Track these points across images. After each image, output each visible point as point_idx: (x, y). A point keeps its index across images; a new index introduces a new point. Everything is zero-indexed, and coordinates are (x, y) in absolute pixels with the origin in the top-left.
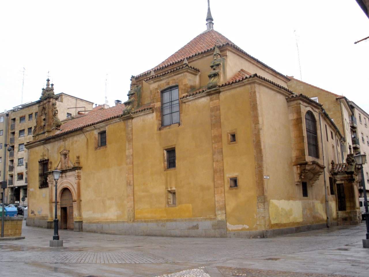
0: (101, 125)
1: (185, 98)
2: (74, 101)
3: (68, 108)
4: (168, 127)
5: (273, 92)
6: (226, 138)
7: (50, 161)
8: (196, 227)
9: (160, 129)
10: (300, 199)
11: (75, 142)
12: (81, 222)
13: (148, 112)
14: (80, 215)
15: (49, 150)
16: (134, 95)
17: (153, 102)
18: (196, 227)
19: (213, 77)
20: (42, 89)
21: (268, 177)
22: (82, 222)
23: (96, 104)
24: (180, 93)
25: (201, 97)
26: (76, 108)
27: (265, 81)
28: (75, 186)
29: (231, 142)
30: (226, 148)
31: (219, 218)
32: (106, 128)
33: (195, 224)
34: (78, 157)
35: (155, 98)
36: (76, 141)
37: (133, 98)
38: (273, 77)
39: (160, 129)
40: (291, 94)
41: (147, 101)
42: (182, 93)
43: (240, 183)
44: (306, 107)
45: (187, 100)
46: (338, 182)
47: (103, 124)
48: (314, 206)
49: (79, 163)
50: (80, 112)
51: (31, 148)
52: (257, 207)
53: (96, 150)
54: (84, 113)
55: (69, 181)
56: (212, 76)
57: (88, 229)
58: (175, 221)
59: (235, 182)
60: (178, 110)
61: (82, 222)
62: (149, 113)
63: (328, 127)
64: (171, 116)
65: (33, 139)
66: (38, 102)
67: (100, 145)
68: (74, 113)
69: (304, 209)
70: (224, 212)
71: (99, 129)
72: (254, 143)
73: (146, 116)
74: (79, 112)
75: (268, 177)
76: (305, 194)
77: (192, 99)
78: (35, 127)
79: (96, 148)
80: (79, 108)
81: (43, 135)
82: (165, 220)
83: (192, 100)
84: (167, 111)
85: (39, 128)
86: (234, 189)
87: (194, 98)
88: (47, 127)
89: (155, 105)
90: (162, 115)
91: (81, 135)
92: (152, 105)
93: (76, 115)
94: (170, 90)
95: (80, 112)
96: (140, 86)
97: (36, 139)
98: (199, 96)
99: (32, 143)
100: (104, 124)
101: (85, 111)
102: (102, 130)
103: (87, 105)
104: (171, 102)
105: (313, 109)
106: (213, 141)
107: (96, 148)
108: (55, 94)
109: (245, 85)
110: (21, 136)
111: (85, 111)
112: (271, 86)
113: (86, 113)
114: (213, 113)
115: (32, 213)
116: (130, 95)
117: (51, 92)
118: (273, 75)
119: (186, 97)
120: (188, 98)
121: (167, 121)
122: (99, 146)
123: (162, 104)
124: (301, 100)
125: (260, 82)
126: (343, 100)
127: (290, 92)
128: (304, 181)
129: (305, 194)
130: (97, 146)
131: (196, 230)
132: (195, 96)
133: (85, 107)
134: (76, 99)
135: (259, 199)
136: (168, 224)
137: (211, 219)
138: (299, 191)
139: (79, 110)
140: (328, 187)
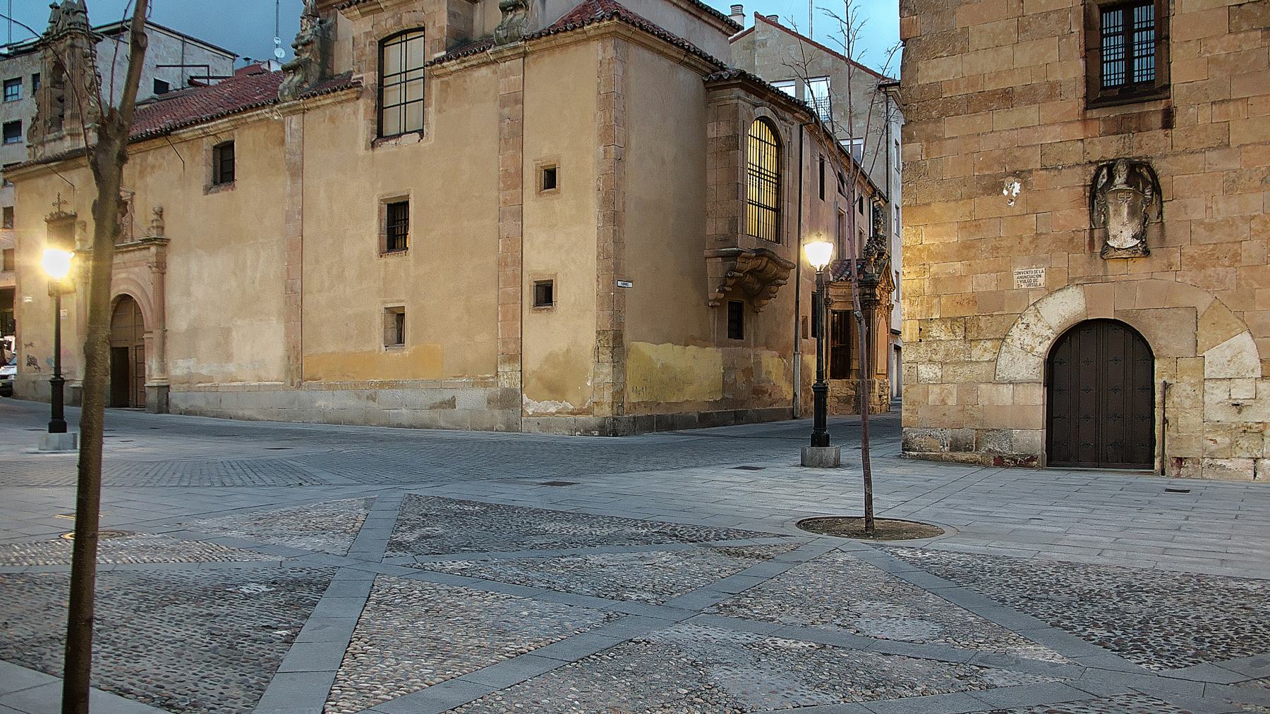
0: (220, 127)
1: (439, 66)
2: (176, 45)
3: (158, 66)
4: (393, 142)
5: (665, 64)
6: (532, 179)
7: (79, 219)
8: (451, 403)
9: (373, 145)
10: (719, 345)
11: (149, 170)
12: (164, 389)
13: (343, 98)
14: (163, 369)
15: (76, 188)
16: (309, 47)
17: (359, 71)
18: (451, 403)
19: (511, 11)
20: (51, 6)
21: (620, 283)
22: (168, 386)
23: (247, 59)
24: (428, 49)
25: (479, 66)
26: (182, 66)
27: (644, 33)
28: (150, 291)
29: (545, 189)
30: (533, 203)
31: (505, 383)
32: (233, 135)
33: (447, 395)
34: (160, 213)
35: (364, 58)
36: (153, 167)
37: (308, 54)
38: (691, 17)
39: (373, 145)
40: (718, 68)
41: (343, 64)
42: (433, 52)
43: (559, 294)
44: (756, 106)
45: (443, 71)
46: (836, 307)
47: (227, 122)
48: (758, 364)
49: (161, 228)
50: (195, 80)
51: (21, 180)
52: (596, 360)
53: (207, 194)
54: (205, 81)
55: (132, 276)
56: (508, 9)
57: (183, 406)
58: (402, 386)
59: (545, 294)
60: (422, 98)
61: (168, 386)
62: (347, 101)
63: (827, 166)
64: (813, 80)
65: (29, 155)
66: (44, 43)
67: (219, 181)
68: (173, 79)
69: (728, 369)
70: (518, 367)
71: (215, 135)
72: (598, 194)
73: (338, 108)
74: (192, 77)
75: (620, 283)
76: (736, 330)
77: (456, 67)
78: (35, 120)
79: (207, 190)
80: (191, 68)
81: (58, 142)
82: (377, 383)
83: (456, 71)
84: (392, 97)
85: (45, 122)
86: (544, 309)
87: (461, 67)
88: (69, 121)
89: (362, 78)
90: (380, 109)
91: (165, 150)
92: (354, 79)
93: (183, 88)
94: (404, 39)
95: (195, 80)
96: (330, 21)
97: (38, 155)
98: (475, 62)
99: (25, 166)
100: (228, 125)
101: (208, 78)
102: (224, 138)
103: (216, 59)
104: (406, 72)
105: (776, 114)
106: (502, 185)
107: (207, 190)
108: (93, 24)
109: (589, 39)
110: (9, 140)
111: (208, 78)
112: (661, 45)
113: (212, 82)
114: (506, 111)
115: (29, 364)
116: (300, 45)
117: (79, 18)
118: (691, 13)
119: (441, 63)
120: (445, 64)
121: (391, 127)
122: (215, 183)
123: (381, 77)
124: (741, 86)
125: (629, 34)
126: (895, 90)
127: (716, 64)
128: (737, 299)
129: (736, 330)
130: (211, 183)
131: (449, 411)
132: (465, 62)
133: (208, 66)
134: (181, 38)
135: (601, 337)
136: (384, 394)
137: (484, 384)
138: (717, 323)
139: (192, 72)
140: (805, 320)
